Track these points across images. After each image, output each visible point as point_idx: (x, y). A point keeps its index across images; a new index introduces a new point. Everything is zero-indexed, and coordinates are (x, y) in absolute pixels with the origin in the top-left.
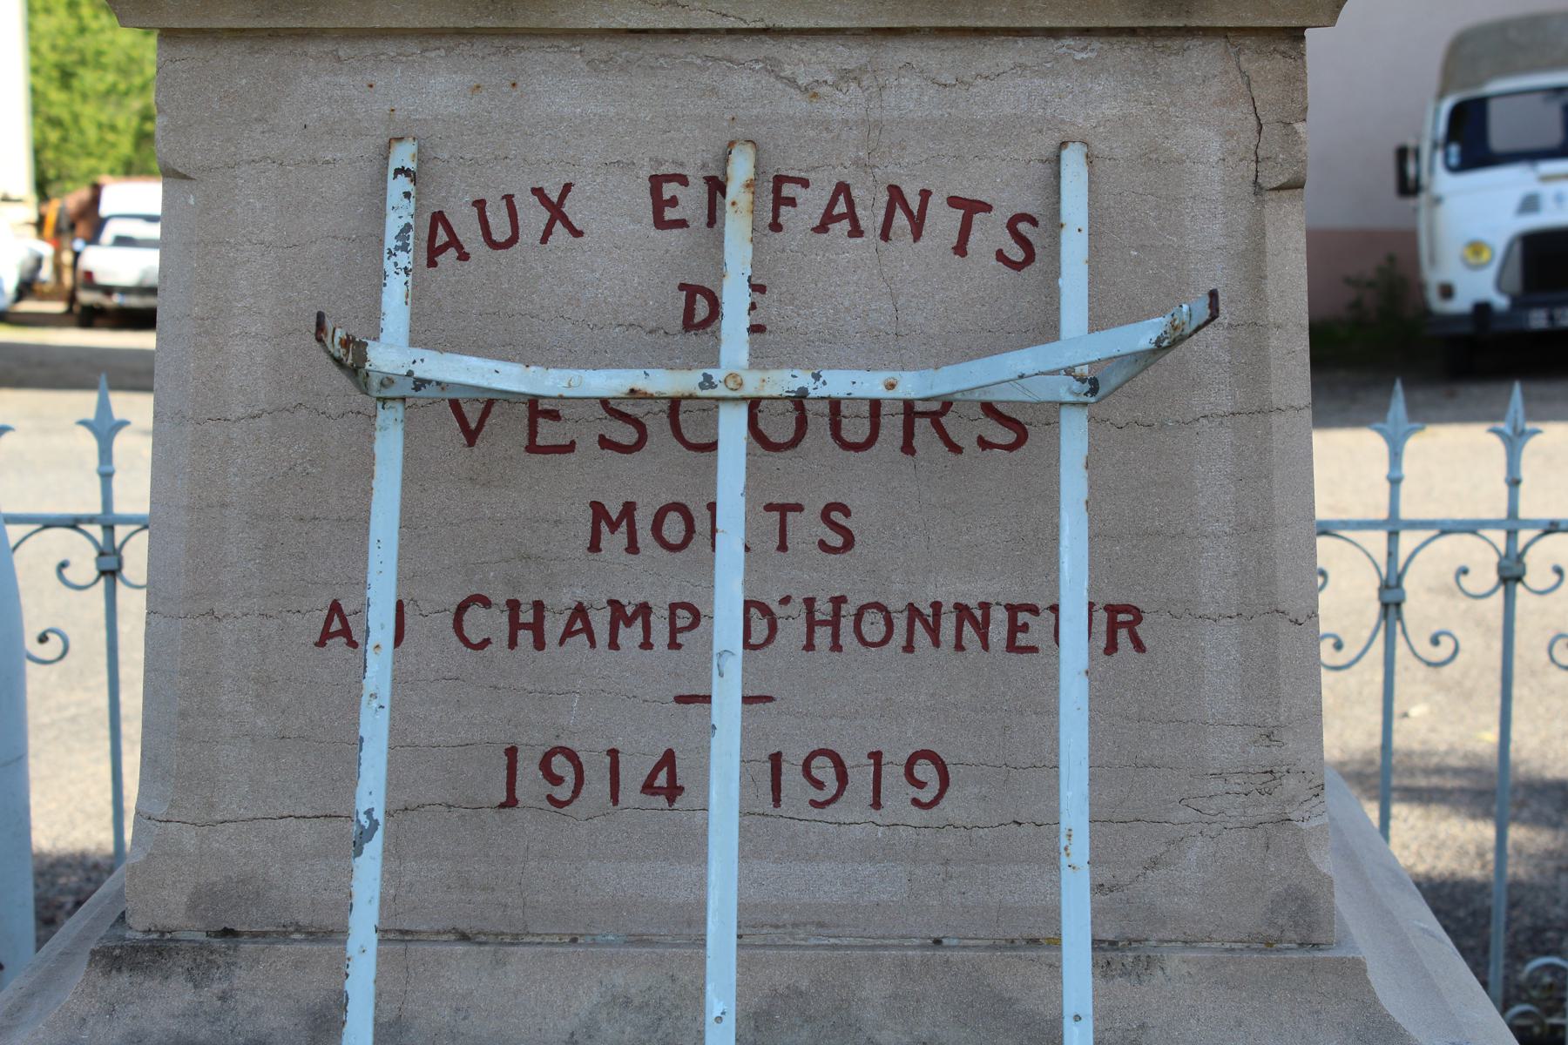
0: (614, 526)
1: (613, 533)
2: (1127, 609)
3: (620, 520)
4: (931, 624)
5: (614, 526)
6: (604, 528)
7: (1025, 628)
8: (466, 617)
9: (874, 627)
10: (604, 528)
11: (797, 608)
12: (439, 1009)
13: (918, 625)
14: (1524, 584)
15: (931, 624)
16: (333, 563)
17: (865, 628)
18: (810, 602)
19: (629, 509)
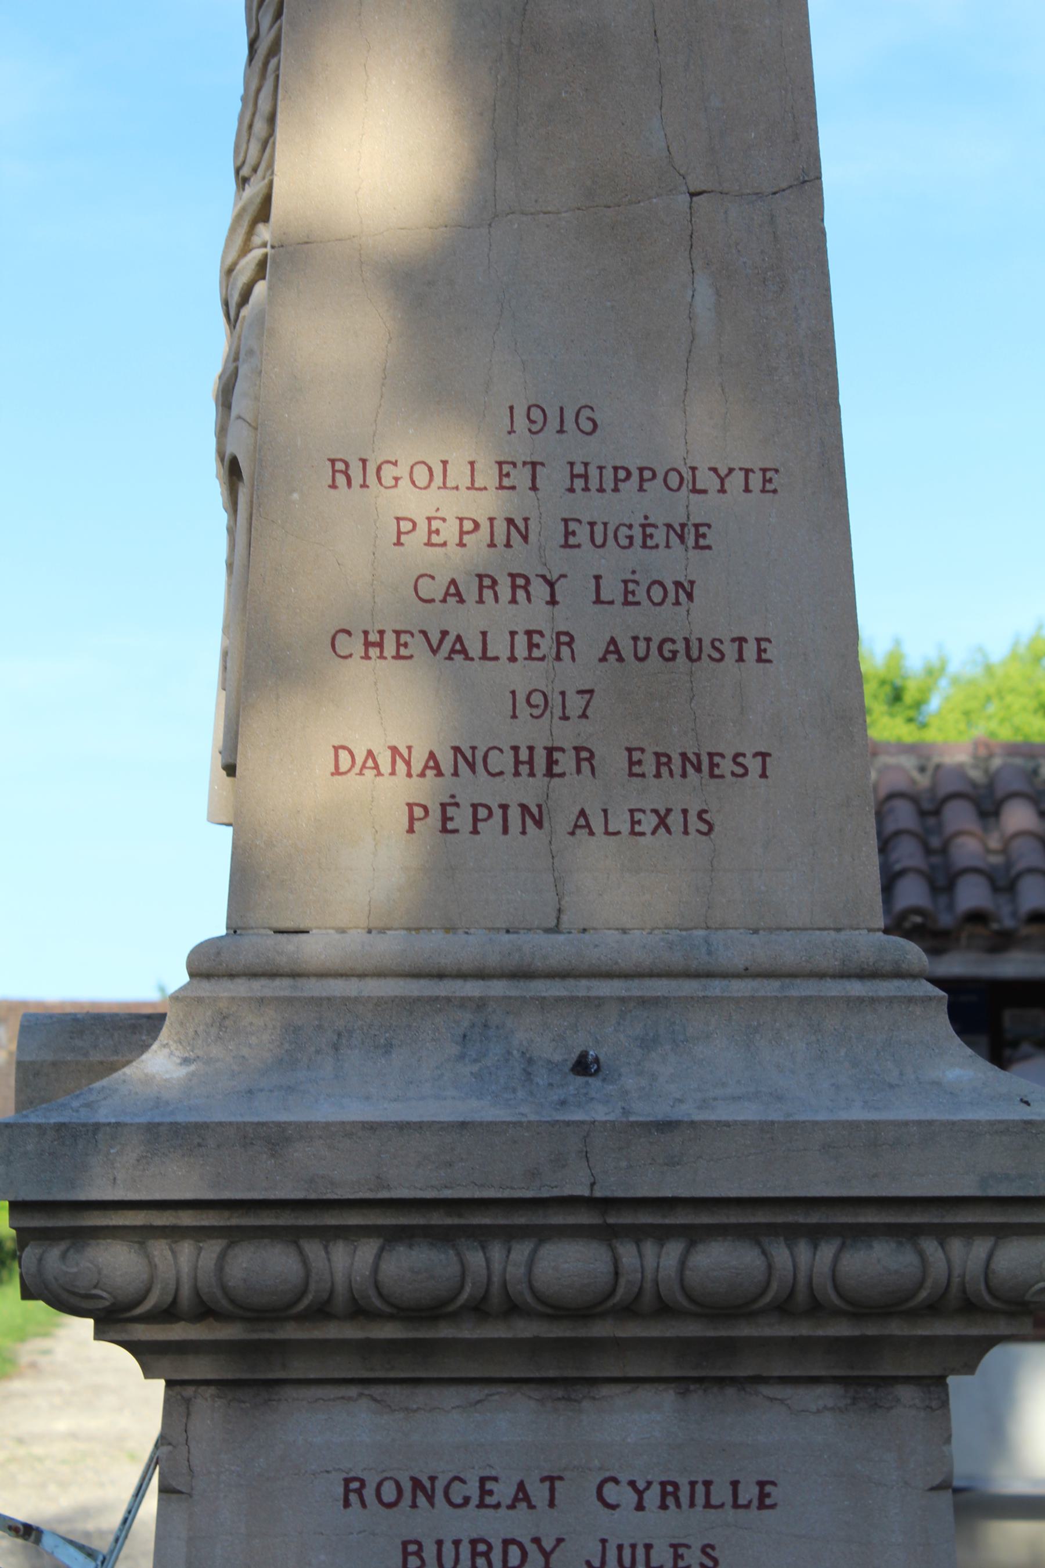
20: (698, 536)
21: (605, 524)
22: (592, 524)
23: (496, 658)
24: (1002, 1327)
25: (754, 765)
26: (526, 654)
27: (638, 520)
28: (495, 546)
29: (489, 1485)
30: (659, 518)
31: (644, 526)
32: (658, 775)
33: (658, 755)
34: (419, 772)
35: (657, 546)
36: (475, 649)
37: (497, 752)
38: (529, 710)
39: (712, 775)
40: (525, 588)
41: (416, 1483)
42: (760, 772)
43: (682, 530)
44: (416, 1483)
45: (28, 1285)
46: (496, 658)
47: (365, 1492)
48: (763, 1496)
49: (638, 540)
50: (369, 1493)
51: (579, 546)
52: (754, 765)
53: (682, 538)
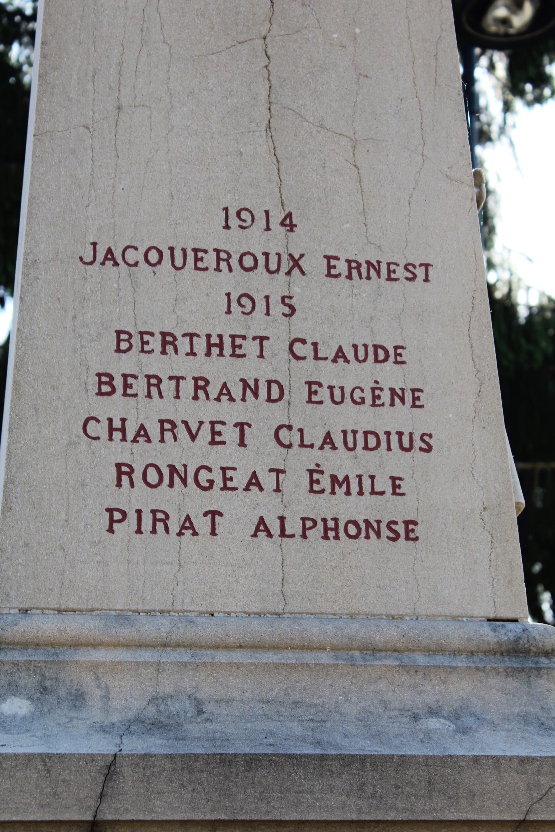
20: (415, 399)
21: (342, 388)
22: (331, 388)
23: (292, 536)
27: (368, 386)
29: (229, 474)
30: (386, 385)
31: (373, 389)
32: (349, 277)
33: (349, 262)
35: (383, 405)
36: (275, 529)
38: (241, 309)
40: (227, 260)
41: (173, 469)
43: (403, 393)
44: (173, 469)
46: (292, 536)
47: (134, 476)
48: (395, 487)
49: (369, 401)
50: (137, 476)
51: (321, 402)
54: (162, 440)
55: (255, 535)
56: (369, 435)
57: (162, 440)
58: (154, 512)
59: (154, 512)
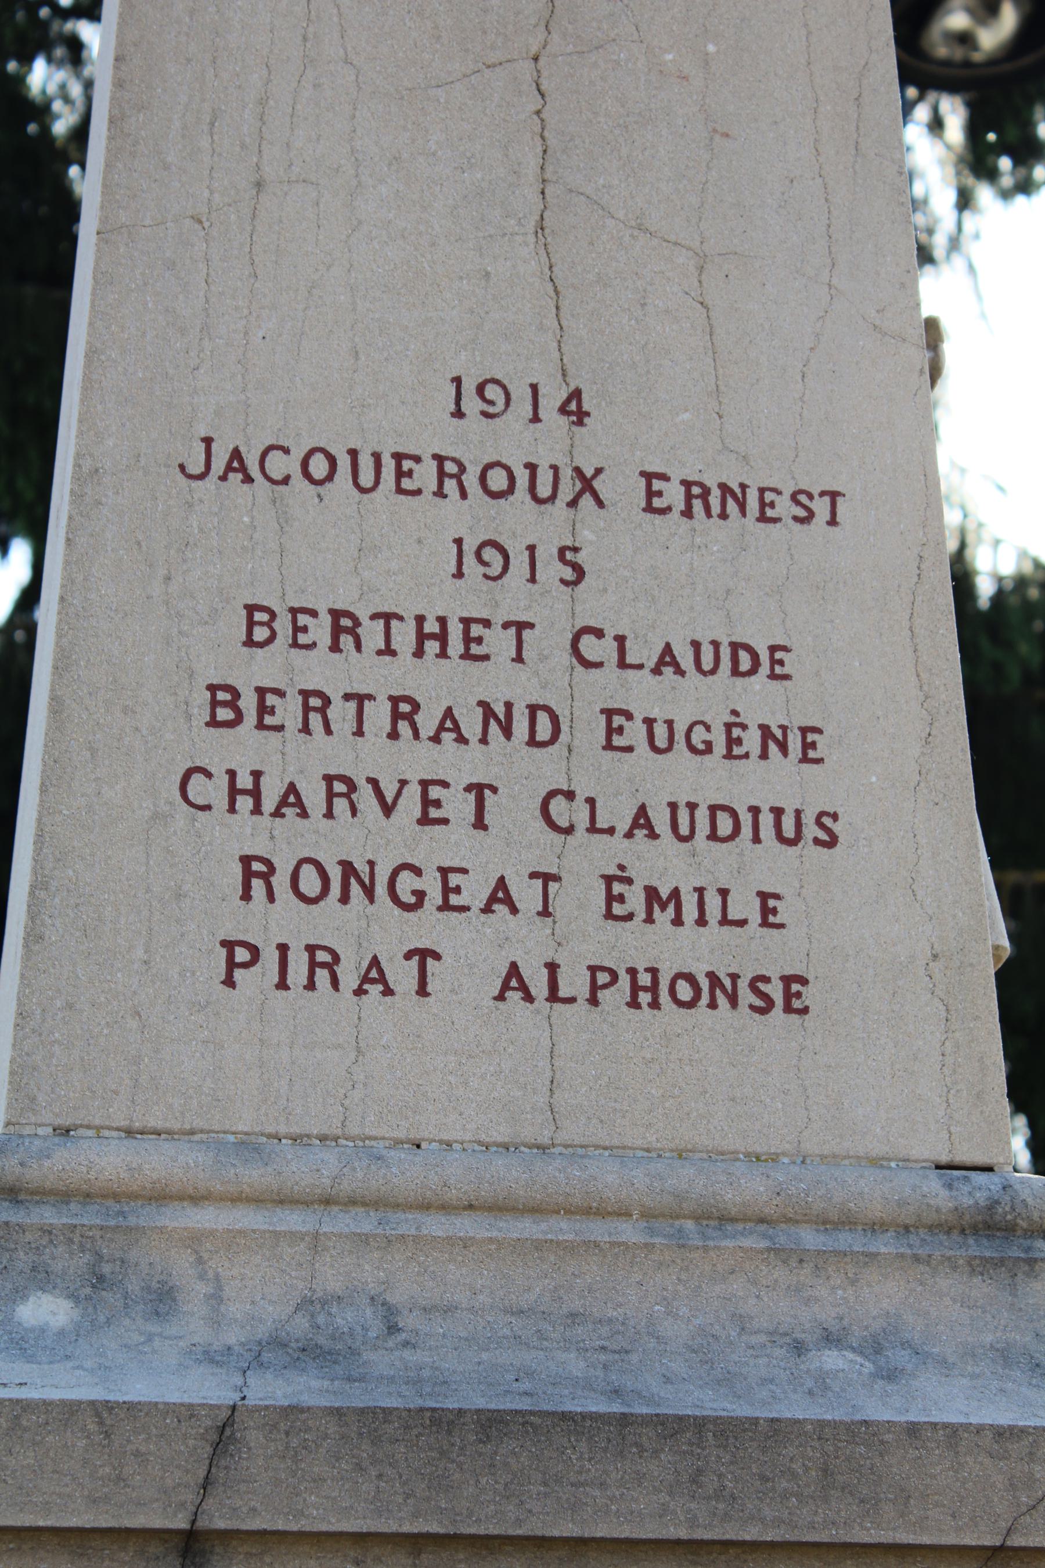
0: (663, 907)
1: (662, 911)
2: (319, 694)
3: (669, 899)
4: (503, 720)
5: (663, 907)
6: (656, 908)
7: (305, 629)
8: (268, 459)
9: (498, 480)
10: (656, 908)
11: (269, 804)
12: (550, 779)
13: (492, 722)
14: (995, 565)
15: (503, 720)
16: (120, 734)
17: (312, 469)
18: (232, 774)
19: (676, 893)
20: (807, 746)
21: (670, 723)
22: (649, 722)
23: (572, 1000)
24: (1007, 67)
25: (821, 507)
26: (461, 650)
28: (393, 653)
30: (753, 718)
31: (729, 727)
34: (272, 811)
35: (746, 756)
37: (278, 453)
39: (763, 518)
41: (348, 869)
42: (828, 518)
44: (348, 869)
45: (830, 1541)
46: (572, 1000)
48: (766, 911)
52: (821, 507)
53: (783, 748)
54: (329, 814)
55: (501, 997)
56: (719, 813)
57: (329, 814)
58: (311, 949)
59: (311, 949)
